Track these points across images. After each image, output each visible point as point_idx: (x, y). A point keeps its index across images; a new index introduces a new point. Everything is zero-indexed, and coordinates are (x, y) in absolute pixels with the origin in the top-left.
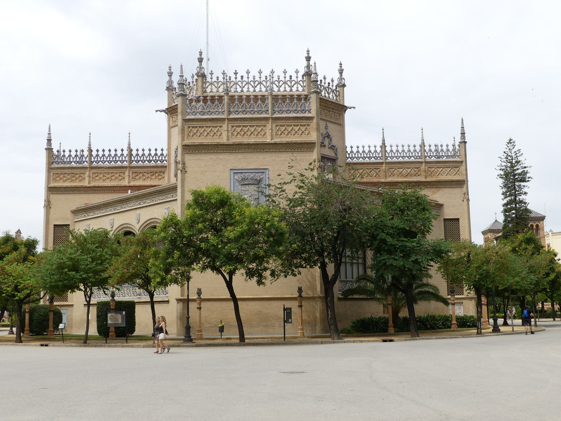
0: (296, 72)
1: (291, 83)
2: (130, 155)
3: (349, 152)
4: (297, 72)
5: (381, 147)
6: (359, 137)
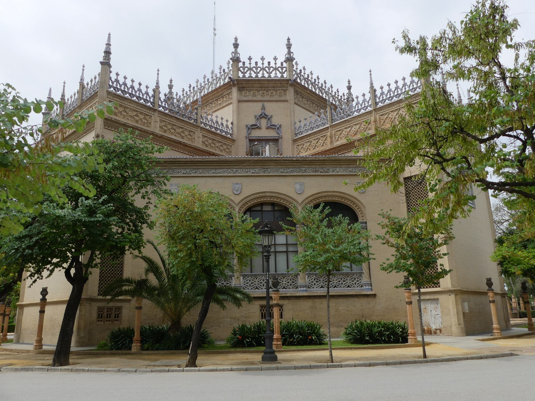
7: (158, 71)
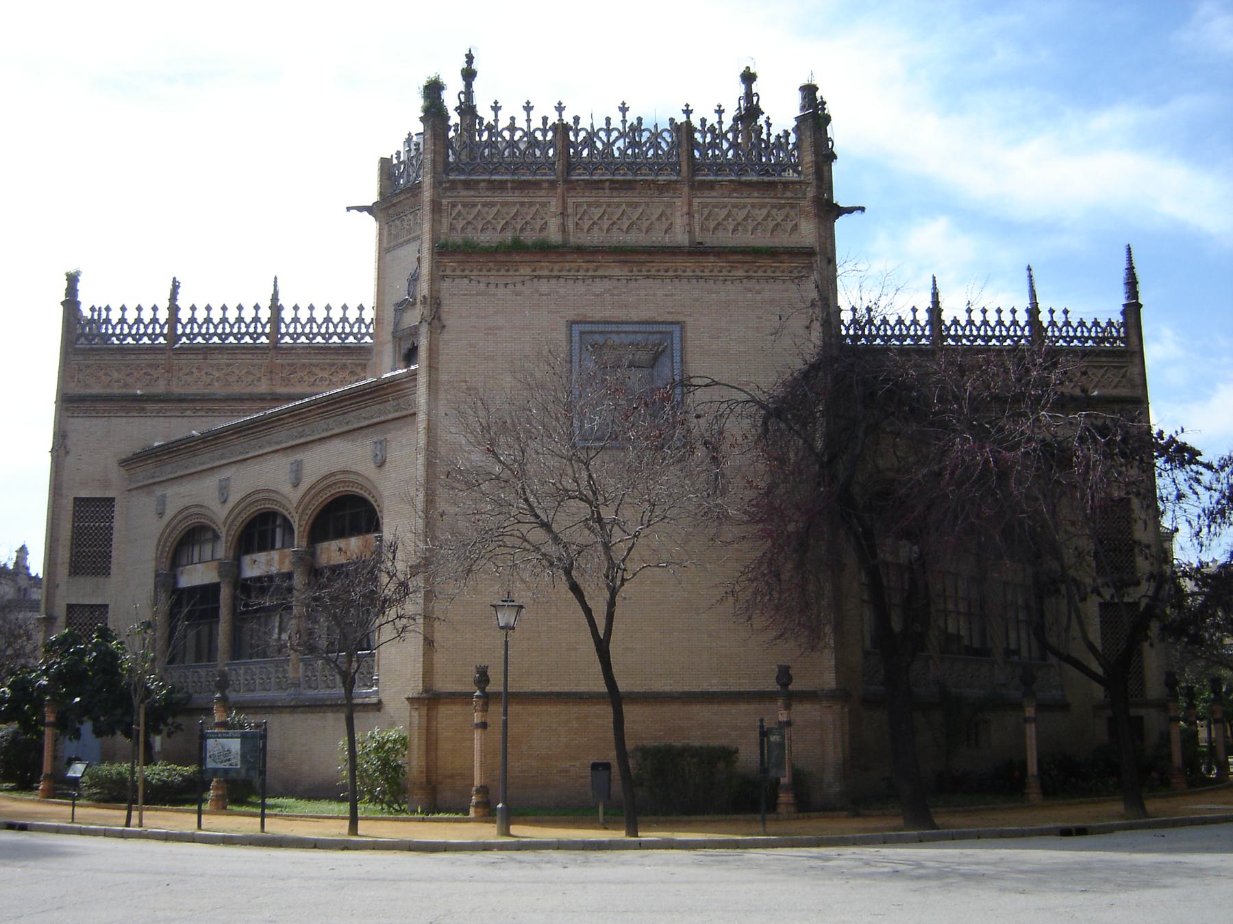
0: (716, 111)
1: (608, 136)
2: (174, 318)
3: (288, 321)
4: (720, 111)
5: (929, 310)
6: (887, 277)
7: (1029, 269)
